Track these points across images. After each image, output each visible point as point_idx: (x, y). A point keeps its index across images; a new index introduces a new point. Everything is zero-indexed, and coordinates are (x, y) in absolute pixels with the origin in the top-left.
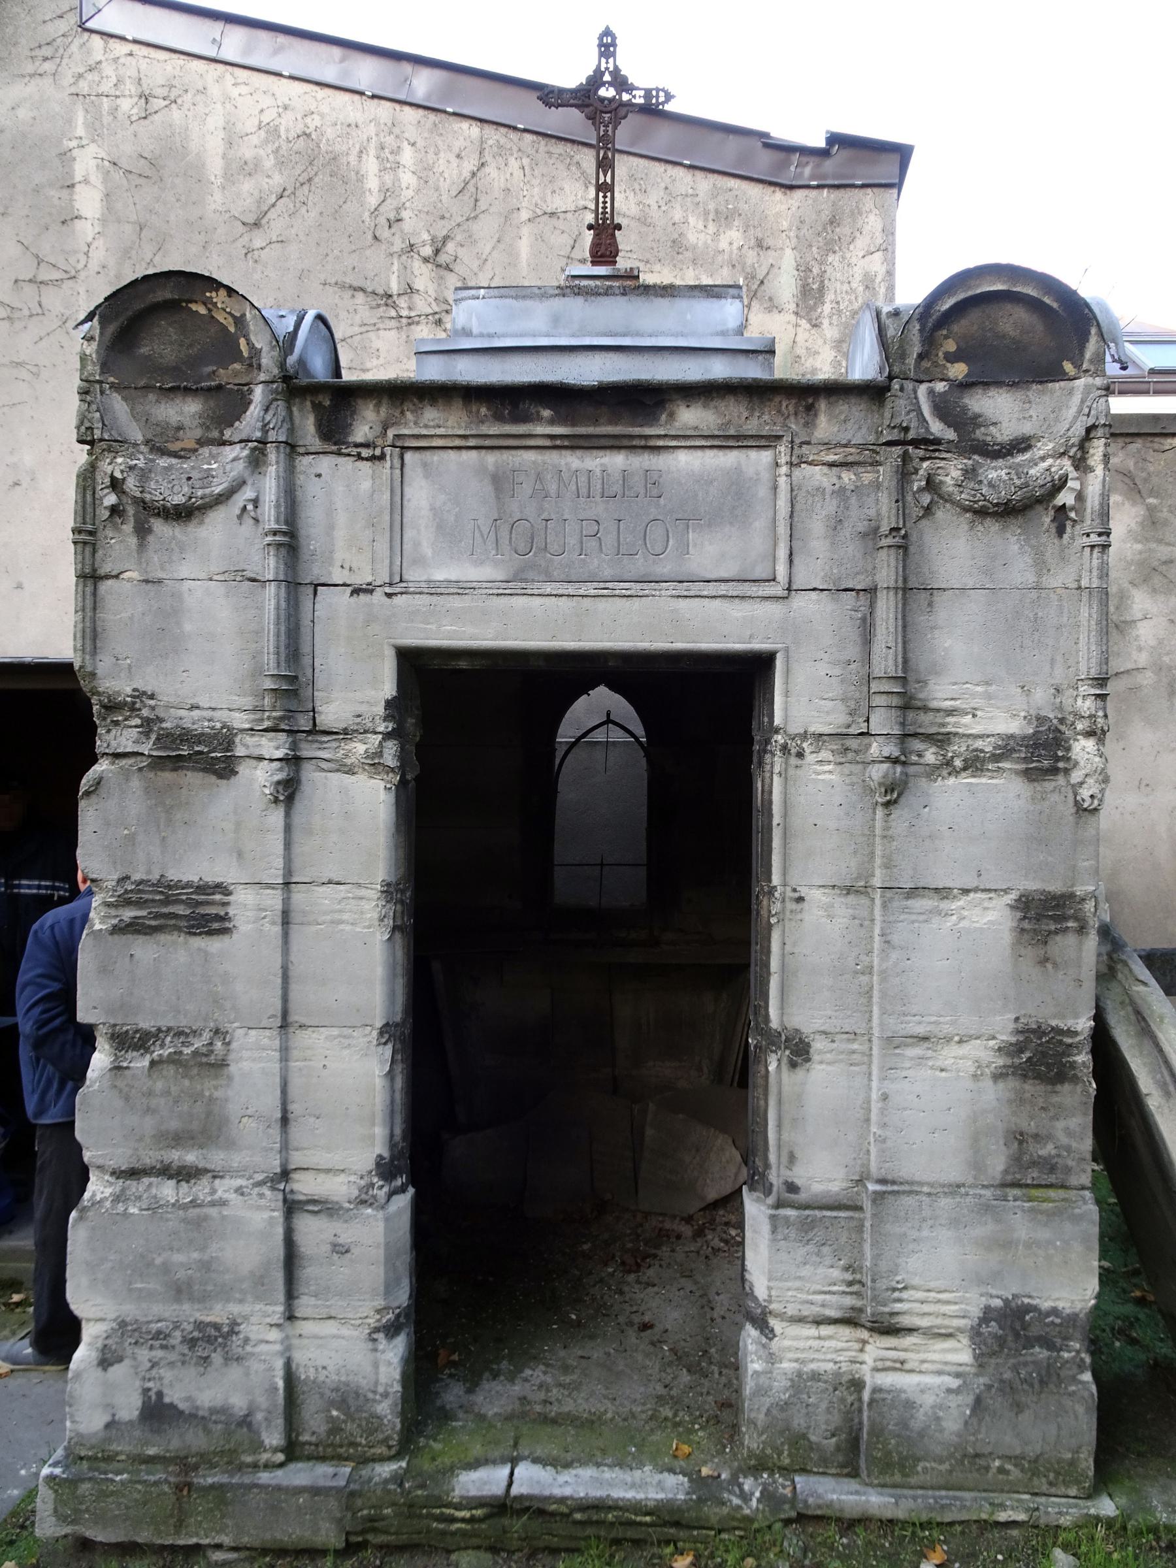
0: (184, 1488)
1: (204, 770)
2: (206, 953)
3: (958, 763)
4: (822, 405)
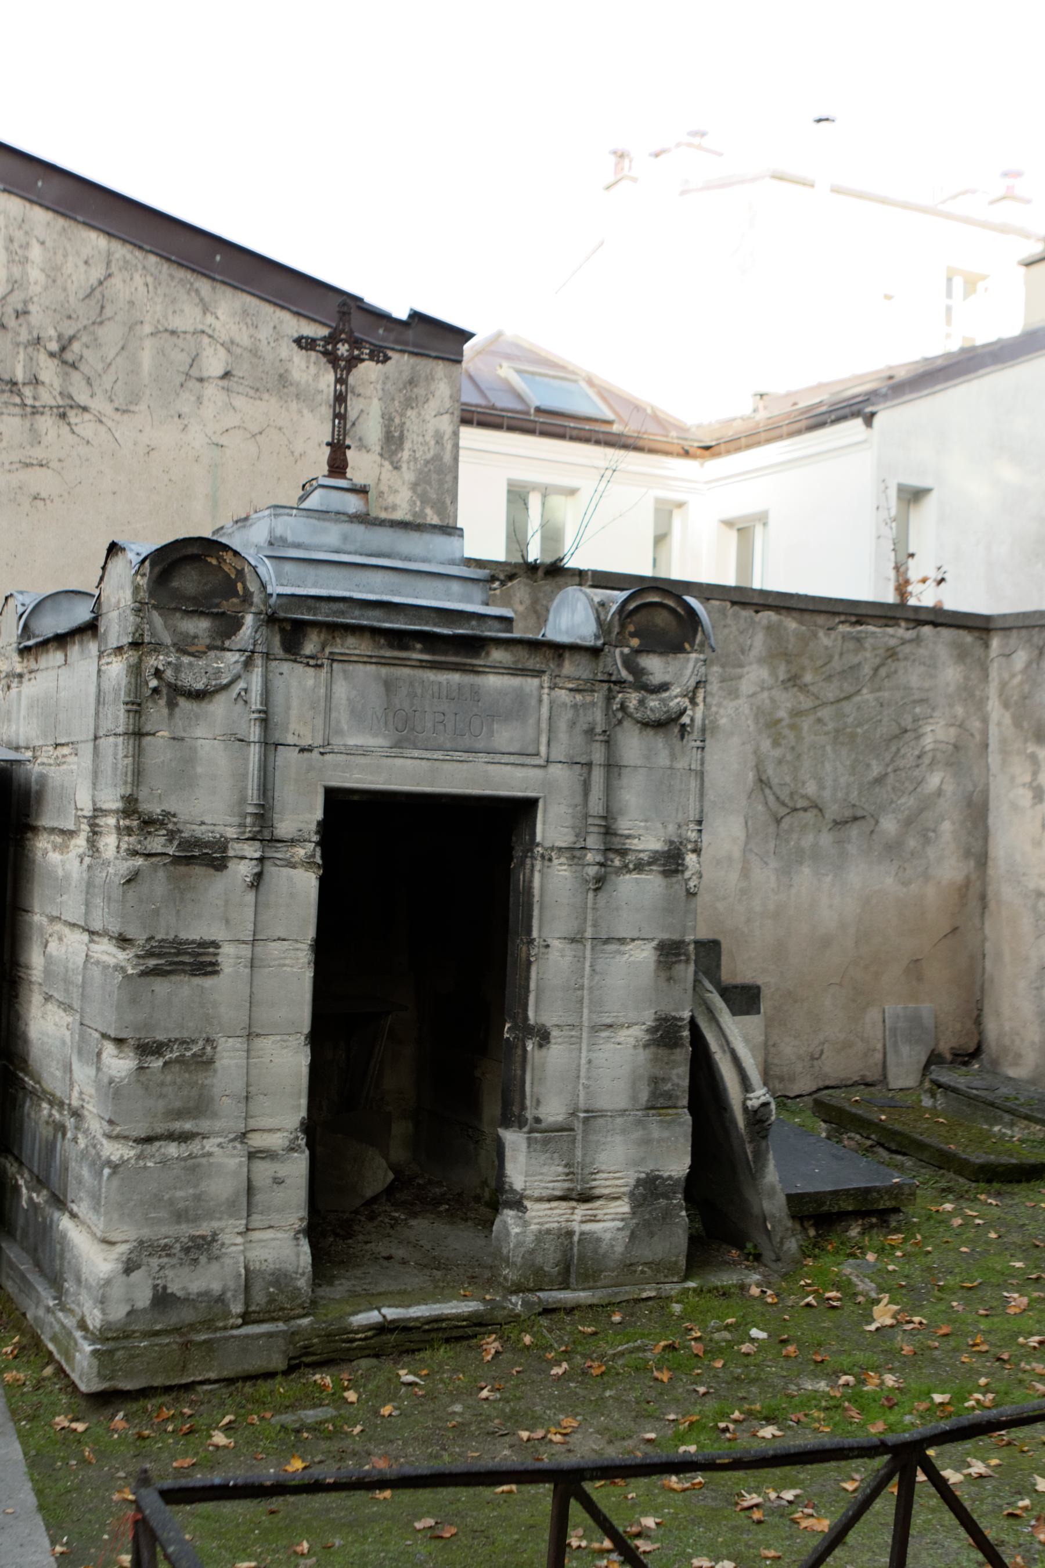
0: (186, 1345)
1: (207, 865)
2: (202, 987)
3: (631, 866)
4: (567, 655)
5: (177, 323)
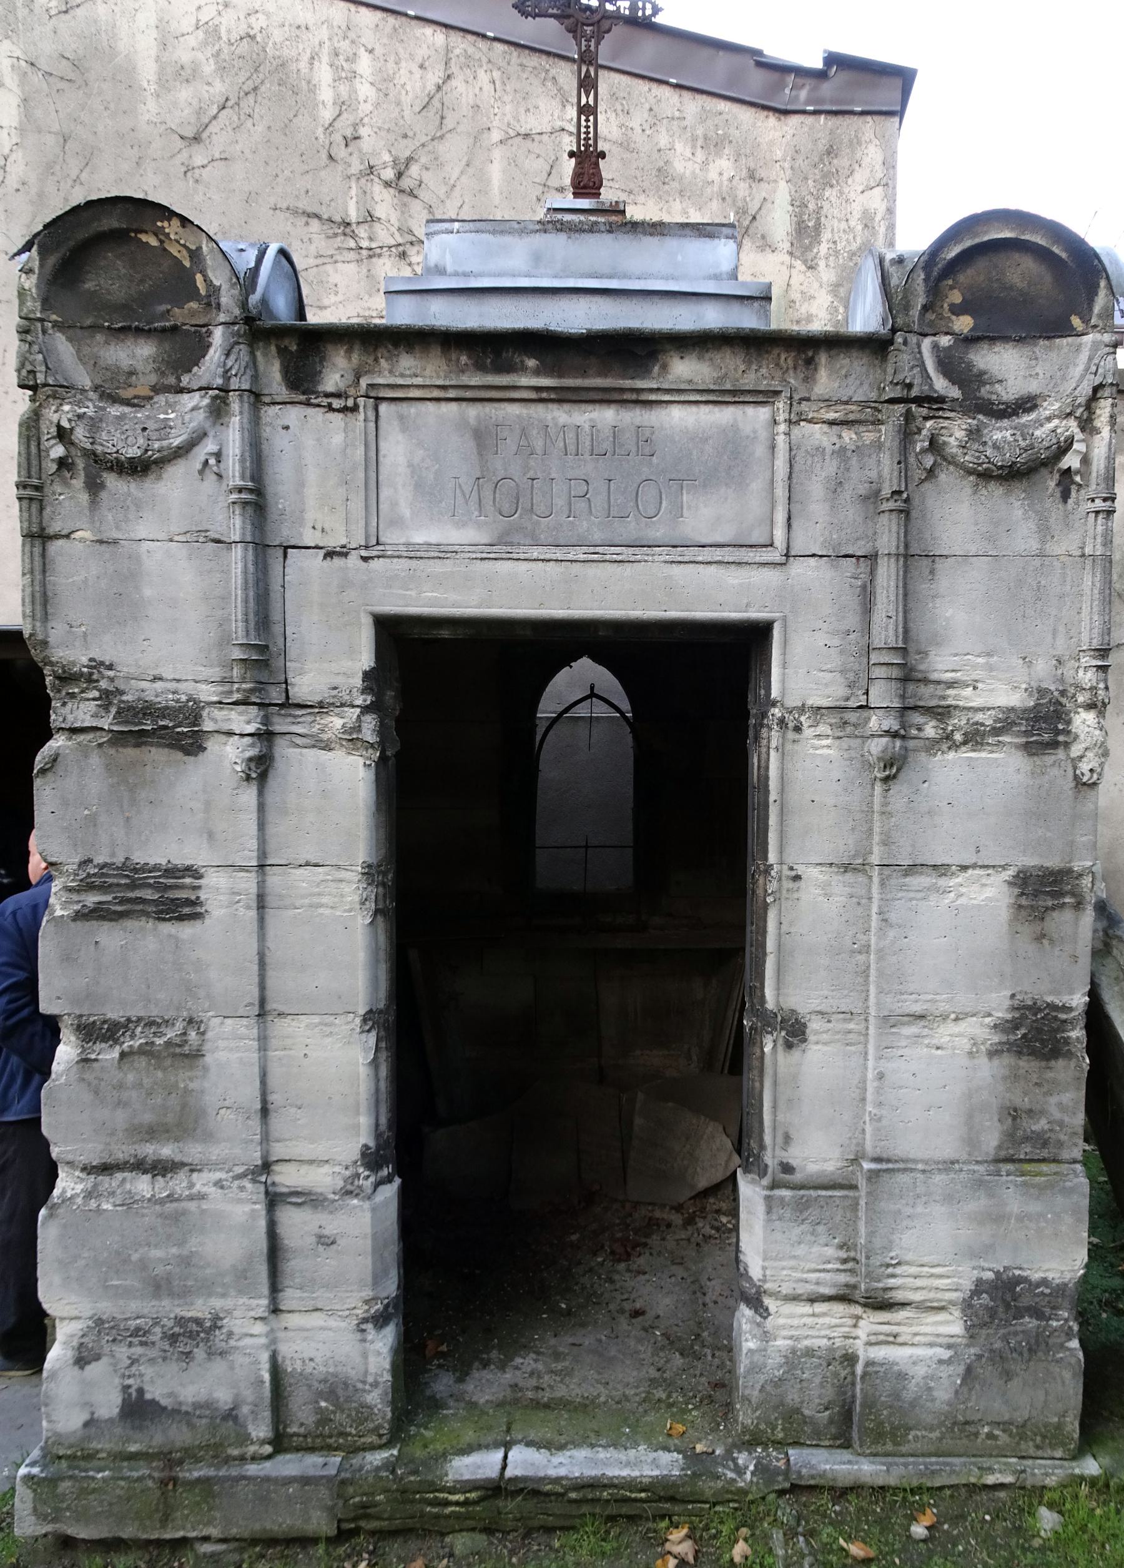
0: (169, 1482)
1: (170, 746)
3: (958, 737)
4: (823, 358)
5: (531, 123)
